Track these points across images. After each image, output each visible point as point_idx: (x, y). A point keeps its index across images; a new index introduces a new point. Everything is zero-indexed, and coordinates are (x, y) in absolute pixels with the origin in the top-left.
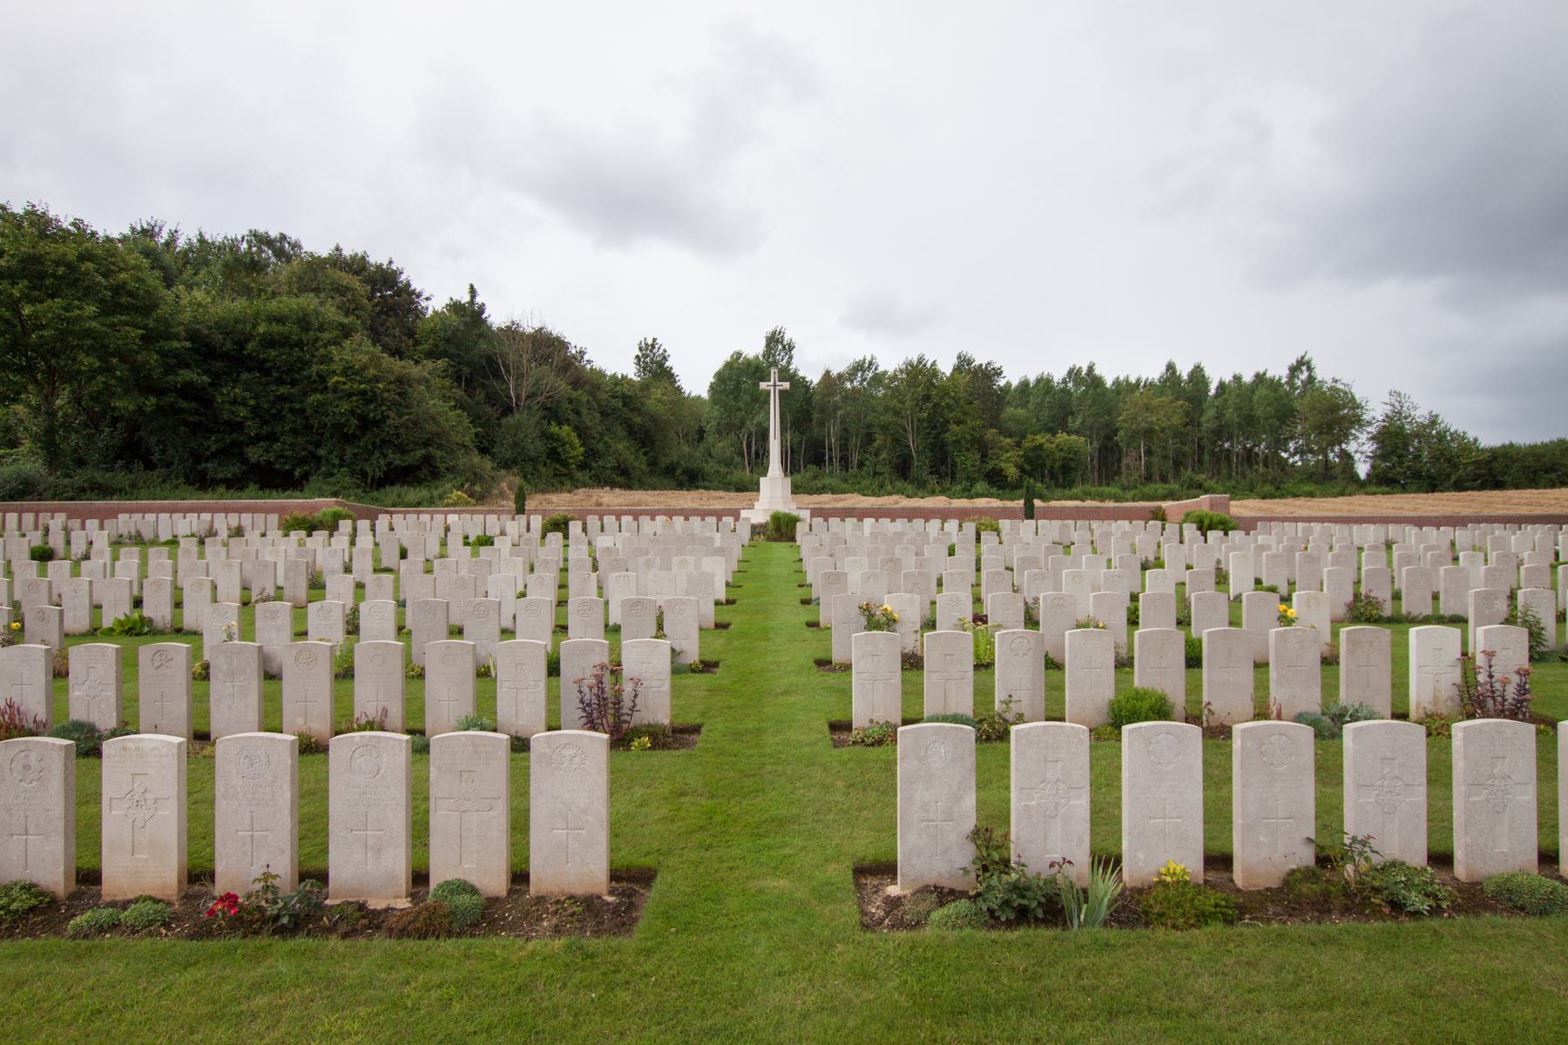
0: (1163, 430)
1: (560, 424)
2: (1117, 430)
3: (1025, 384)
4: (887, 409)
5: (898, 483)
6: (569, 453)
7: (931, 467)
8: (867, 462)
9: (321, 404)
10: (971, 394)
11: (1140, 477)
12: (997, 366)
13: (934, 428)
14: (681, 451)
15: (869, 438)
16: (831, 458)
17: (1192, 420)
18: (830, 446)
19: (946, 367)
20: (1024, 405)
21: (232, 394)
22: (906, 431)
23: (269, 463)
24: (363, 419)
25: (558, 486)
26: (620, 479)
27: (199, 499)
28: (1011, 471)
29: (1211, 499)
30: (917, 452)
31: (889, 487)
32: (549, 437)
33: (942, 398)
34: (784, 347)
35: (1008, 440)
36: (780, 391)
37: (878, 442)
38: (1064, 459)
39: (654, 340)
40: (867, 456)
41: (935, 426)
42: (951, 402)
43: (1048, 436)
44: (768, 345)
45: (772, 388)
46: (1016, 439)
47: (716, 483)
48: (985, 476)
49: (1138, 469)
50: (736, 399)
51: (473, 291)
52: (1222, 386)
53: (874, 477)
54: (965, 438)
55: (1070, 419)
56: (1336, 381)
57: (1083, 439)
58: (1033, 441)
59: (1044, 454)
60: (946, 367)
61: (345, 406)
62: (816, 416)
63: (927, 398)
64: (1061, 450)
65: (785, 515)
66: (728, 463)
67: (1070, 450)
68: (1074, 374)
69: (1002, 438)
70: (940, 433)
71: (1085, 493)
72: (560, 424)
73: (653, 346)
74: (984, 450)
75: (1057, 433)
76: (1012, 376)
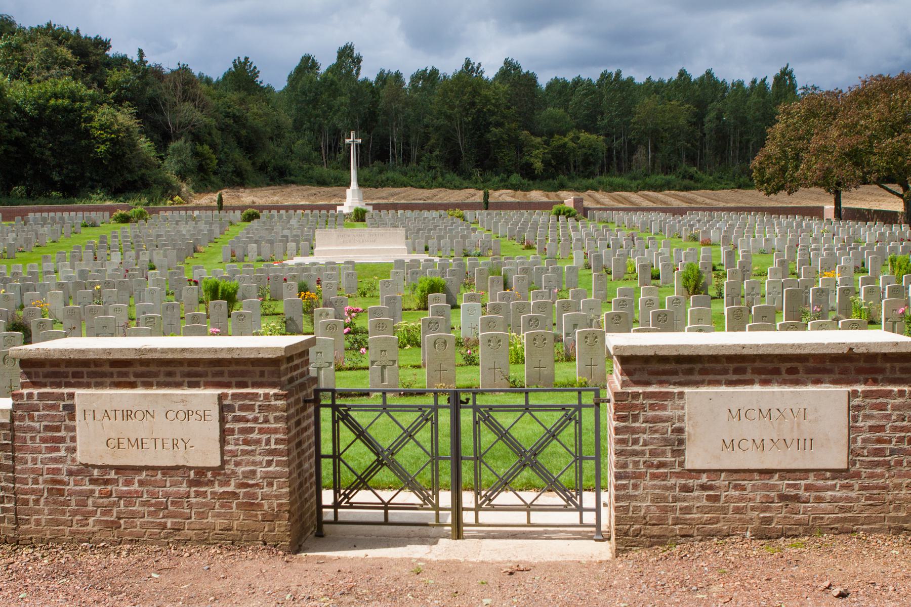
1: (202, 144)
5: (448, 175)
7: (477, 161)
8: (424, 158)
14: (273, 151)
15: (427, 137)
17: (698, 120)
18: (393, 142)
19: (490, 73)
26: (238, 180)
28: (538, 165)
30: (465, 149)
31: (440, 179)
33: (485, 105)
34: (353, 61)
35: (539, 140)
37: (433, 141)
39: (246, 59)
41: (480, 125)
44: (339, 57)
46: (545, 138)
47: (301, 178)
48: (522, 168)
50: (315, 108)
51: (141, 53)
53: (429, 171)
54: (502, 138)
55: (599, 118)
56: (815, 89)
60: (490, 73)
62: (381, 118)
63: (473, 104)
65: (362, 209)
66: (307, 159)
67: (590, 147)
69: (533, 138)
71: (600, 183)
72: (202, 144)
73: (245, 63)
74: (520, 147)
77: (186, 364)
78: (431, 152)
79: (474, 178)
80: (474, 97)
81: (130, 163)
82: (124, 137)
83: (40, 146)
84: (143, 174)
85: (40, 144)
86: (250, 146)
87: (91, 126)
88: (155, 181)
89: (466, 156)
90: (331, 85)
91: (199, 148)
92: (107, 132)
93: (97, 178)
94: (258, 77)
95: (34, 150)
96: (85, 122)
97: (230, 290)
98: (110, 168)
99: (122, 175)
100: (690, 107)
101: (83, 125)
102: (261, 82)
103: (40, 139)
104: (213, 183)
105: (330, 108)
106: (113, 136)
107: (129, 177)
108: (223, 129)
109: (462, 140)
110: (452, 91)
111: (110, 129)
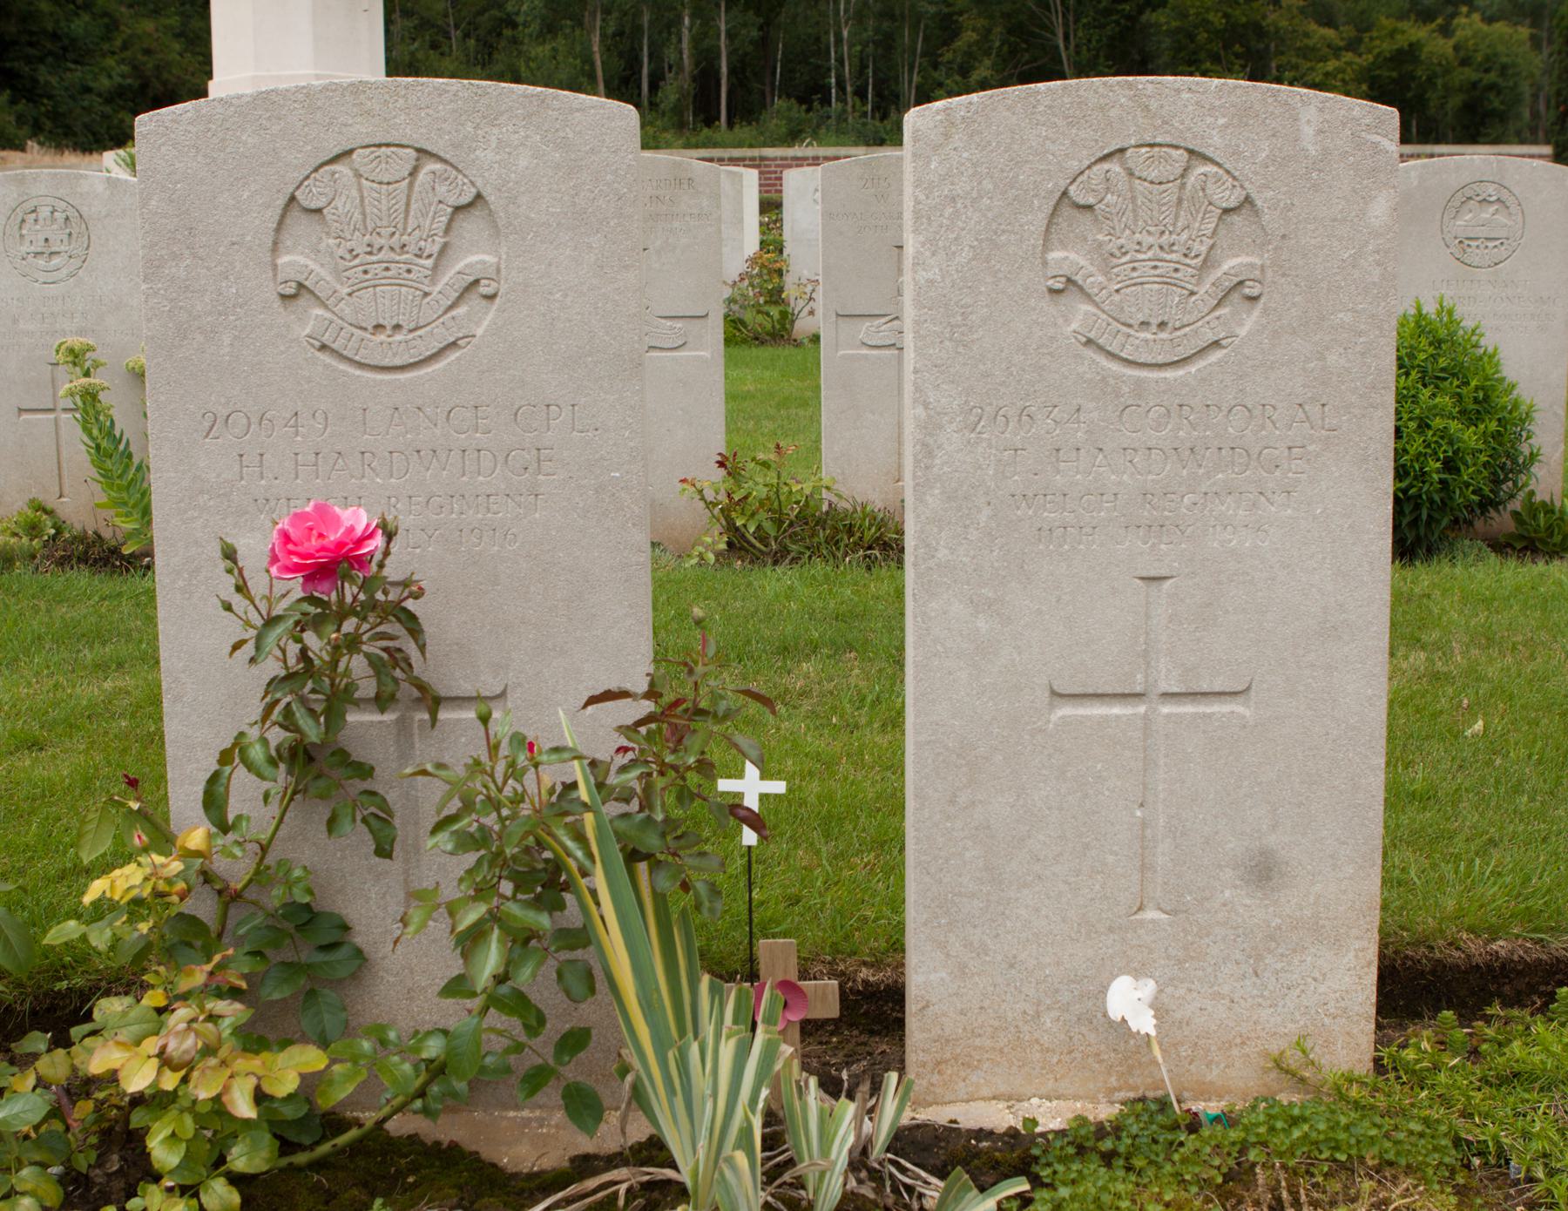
16: (841, 86)
19: (67, 153)
29: (763, 1022)
37: (969, 36)
38: (1474, 85)
58: (1392, 34)
59: (1421, 73)
69: (1313, 26)
109: (1066, 37)
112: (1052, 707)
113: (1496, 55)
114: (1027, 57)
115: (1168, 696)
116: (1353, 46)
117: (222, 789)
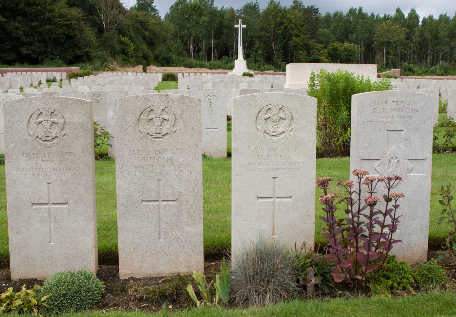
0: (395, 42)
1: (123, 36)
2: (373, 41)
3: (328, 16)
4: (261, 30)
6: (128, 49)
7: (283, 58)
9: (50, 30)
10: (303, 22)
11: (383, 65)
12: (316, 7)
13: (284, 38)
14: (161, 49)
20: (328, 27)
21: (15, 26)
22: (271, 40)
23: (29, 54)
24: (67, 36)
25: (126, 64)
27: (6, 68)
30: (276, 50)
32: (121, 42)
33: (289, 24)
36: (242, 28)
40: (251, 52)
42: (293, 26)
43: (340, 44)
45: (239, 27)
49: (383, 60)
52: (424, 21)
53: (255, 63)
54: (299, 44)
55: (350, 35)
57: (357, 46)
58: (333, 46)
61: (61, 31)
62: (225, 31)
63: (281, 24)
64: (346, 51)
68: (352, 11)
69: (318, 44)
70: (287, 41)
75: (344, 42)
76: (323, 13)
77: (105, 179)
78: (256, 51)
79: (282, 68)
80: (282, 19)
81: (79, 42)
82: (75, 24)
83: (16, 29)
84: (87, 51)
85: (16, 28)
86: (151, 43)
87: (53, 16)
88: (95, 56)
89: (277, 55)
90: (198, 9)
91: (123, 39)
92: (64, 20)
93: (56, 53)
94: (153, 3)
95: (11, 32)
96: (48, 12)
97: (356, 85)
98: (65, 46)
99: (73, 51)
100: (406, 29)
101: (47, 14)
102: (155, 6)
103: (17, 24)
104: (131, 62)
105: (197, 23)
106: (68, 22)
107: (78, 52)
108: (137, 30)
109: (274, 45)
110: (270, 15)
111: (66, 18)
112: (32, 206)
113: (351, 49)
114: (267, 49)
115: (54, 204)
116: (325, 47)
117: (167, 285)
